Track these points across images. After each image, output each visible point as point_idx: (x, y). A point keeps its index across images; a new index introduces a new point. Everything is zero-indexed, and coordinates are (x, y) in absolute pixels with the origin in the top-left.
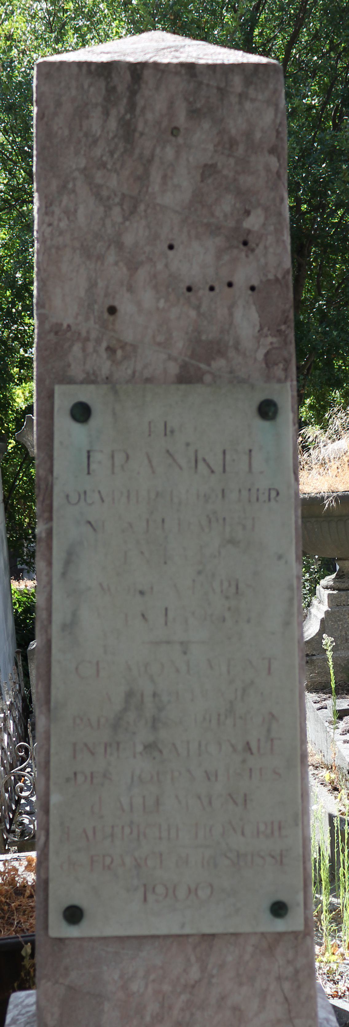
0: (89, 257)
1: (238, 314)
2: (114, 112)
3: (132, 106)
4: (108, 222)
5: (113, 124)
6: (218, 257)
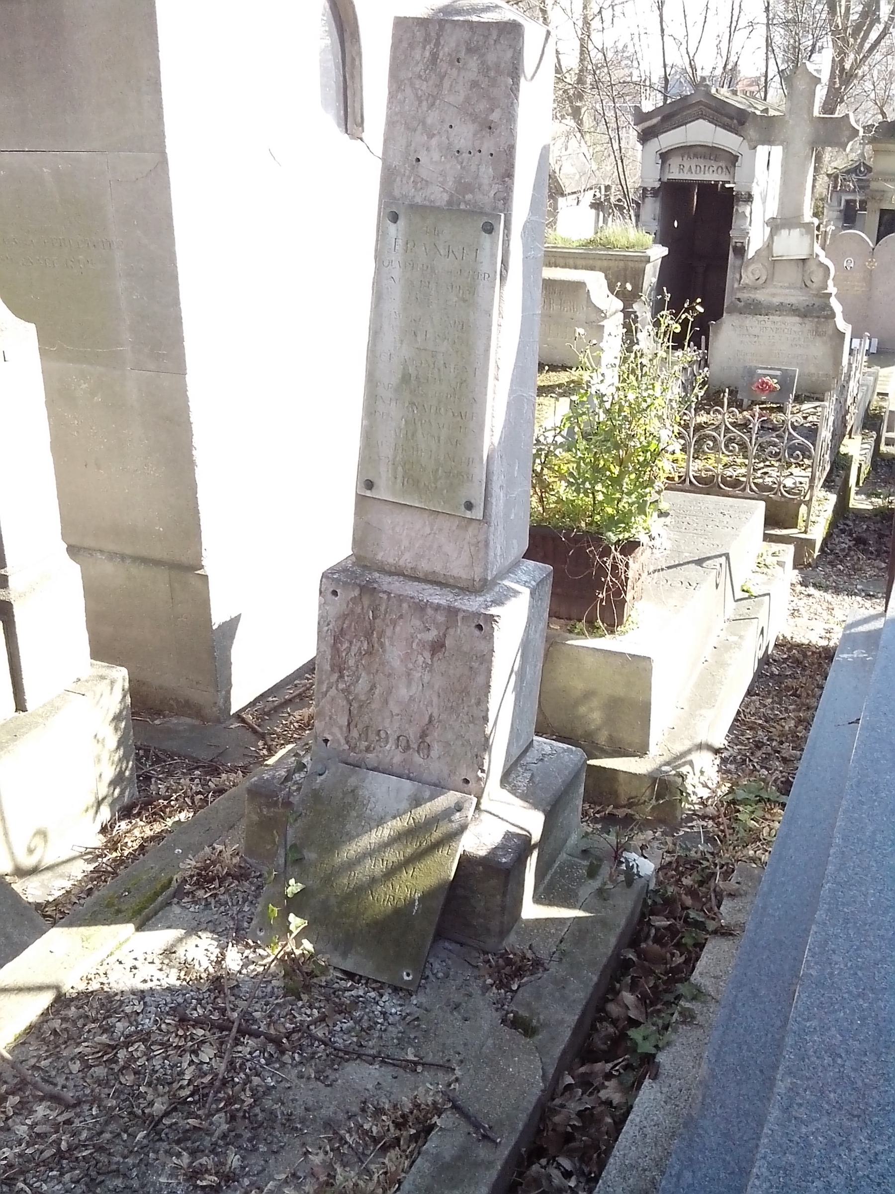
0: (408, 129)
1: (483, 169)
2: (428, 47)
3: (437, 44)
4: (420, 111)
5: (427, 54)
6: (475, 135)
